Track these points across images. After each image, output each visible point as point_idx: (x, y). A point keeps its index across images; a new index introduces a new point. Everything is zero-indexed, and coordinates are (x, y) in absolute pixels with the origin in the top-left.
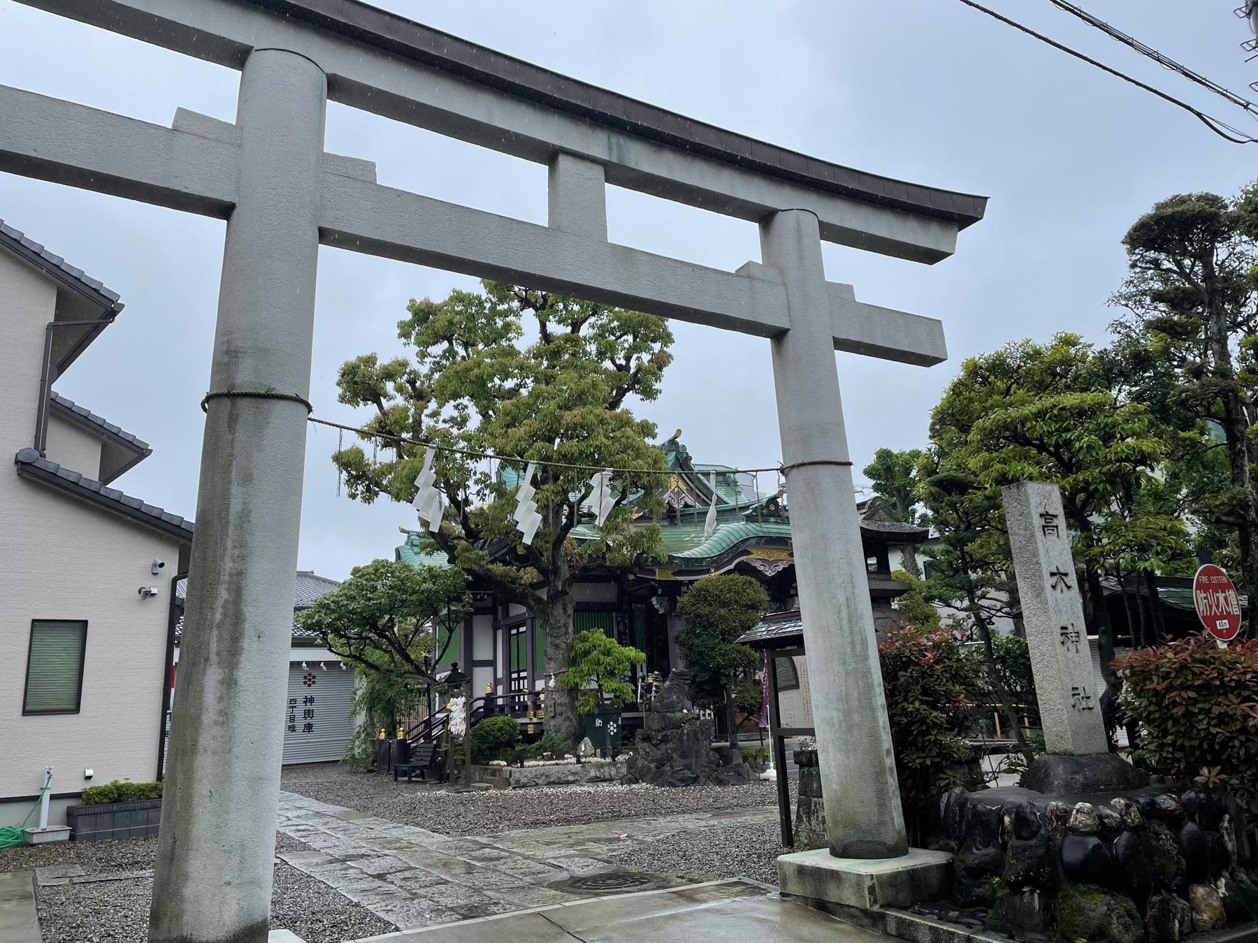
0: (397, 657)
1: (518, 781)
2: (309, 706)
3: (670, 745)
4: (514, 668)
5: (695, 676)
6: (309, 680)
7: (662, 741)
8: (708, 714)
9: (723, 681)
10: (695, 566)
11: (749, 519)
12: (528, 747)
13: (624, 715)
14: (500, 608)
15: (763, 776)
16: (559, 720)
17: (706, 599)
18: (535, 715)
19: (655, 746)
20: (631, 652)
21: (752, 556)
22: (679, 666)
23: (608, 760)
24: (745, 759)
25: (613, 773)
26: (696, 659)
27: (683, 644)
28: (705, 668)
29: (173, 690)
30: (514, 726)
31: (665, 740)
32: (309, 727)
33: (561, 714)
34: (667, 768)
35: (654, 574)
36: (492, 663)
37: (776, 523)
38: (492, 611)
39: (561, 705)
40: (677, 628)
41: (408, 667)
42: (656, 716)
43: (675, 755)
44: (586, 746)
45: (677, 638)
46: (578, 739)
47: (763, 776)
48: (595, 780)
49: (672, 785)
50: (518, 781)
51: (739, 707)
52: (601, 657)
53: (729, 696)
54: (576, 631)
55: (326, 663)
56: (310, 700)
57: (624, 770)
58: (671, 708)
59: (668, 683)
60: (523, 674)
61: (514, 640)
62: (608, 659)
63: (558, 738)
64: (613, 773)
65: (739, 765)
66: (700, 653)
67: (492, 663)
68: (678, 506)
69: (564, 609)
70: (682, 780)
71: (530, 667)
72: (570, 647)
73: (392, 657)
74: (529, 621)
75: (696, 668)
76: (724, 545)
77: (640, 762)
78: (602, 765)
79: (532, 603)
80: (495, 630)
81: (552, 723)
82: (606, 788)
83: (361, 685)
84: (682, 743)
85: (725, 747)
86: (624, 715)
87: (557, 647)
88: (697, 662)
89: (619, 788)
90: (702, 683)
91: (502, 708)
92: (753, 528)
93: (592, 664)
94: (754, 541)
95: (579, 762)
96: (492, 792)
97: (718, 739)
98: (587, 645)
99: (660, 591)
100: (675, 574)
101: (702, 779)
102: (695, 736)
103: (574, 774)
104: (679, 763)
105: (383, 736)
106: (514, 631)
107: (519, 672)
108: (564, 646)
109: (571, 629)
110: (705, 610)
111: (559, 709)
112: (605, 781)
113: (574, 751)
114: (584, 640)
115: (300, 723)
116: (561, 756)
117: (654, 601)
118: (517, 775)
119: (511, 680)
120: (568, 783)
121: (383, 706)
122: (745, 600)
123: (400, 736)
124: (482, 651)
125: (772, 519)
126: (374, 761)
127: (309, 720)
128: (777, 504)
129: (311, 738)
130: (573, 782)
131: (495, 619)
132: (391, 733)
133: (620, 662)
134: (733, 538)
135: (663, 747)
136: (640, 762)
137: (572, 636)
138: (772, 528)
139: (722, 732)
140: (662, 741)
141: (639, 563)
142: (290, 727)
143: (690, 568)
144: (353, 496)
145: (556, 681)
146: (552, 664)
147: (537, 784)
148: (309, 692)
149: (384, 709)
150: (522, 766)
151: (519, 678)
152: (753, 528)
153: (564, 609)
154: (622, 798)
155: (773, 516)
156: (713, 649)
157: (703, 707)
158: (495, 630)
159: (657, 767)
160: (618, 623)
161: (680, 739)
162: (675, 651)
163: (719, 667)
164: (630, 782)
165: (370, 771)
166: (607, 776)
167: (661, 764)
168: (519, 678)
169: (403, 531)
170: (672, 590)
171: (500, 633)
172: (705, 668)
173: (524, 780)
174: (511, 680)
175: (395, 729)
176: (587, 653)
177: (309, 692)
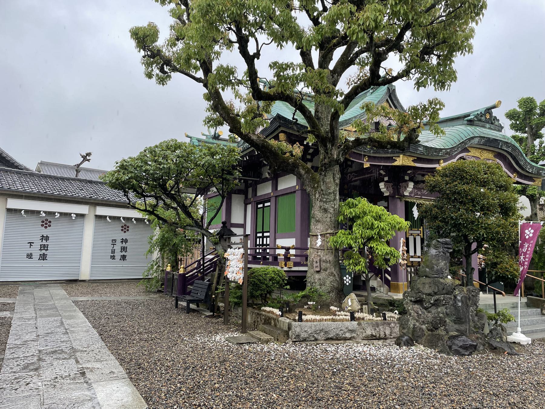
0: (183, 216)
1: (298, 336)
2: (124, 245)
4: (259, 229)
6: (125, 229)
7: (433, 305)
11: (471, 123)
14: (250, 190)
16: (323, 275)
18: (286, 265)
19: (426, 309)
21: (469, 154)
25: (388, 332)
29: (249, 242)
31: (436, 304)
32: (124, 258)
33: (325, 270)
36: (243, 226)
37: (490, 128)
38: (244, 192)
41: (188, 221)
44: (352, 301)
50: (298, 336)
55: (136, 219)
56: (125, 241)
60: (265, 234)
61: (260, 212)
63: (323, 290)
64: (388, 332)
71: (272, 230)
73: (178, 214)
74: (273, 200)
79: (303, 172)
80: (246, 205)
81: (317, 276)
83: (157, 233)
87: (326, 210)
95: (353, 318)
96: (274, 346)
99: (386, 179)
103: (352, 331)
104: (453, 329)
105: (169, 269)
106: (260, 206)
107: (263, 232)
108: (331, 210)
111: (324, 265)
112: (379, 339)
115: (118, 254)
118: (298, 330)
119: (257, 237)
120: (345, 339)
121: (171, 248)
123: (181, 271)
124: (237, 217)
125: (488, 125)
126: (162, 285)
127: (124, 253)
128: (491, 114)
129: (124, 264)
130: (350, 339)
131: (246, 197)
132: (175, 267)
134: (455, 140)
135: (433, 310)
140: (433, 305)
142: (111, 257)
144: (149, 76)
145: (323, 241)
146: (319, 226)
147: (316, 340)
148: (125, 236)
149: (170, 251)
151: (263, 237)
155: (488, 123)
158: (246, 205)
165: (159, 291)
166: (382, 335)
167: (434, 327)
168: (263, 237)
169: (187, 136)
171: (249, 207)
173: (304, 335)
174: (257, 237)
175: (177, 264)
177: (125, 236)
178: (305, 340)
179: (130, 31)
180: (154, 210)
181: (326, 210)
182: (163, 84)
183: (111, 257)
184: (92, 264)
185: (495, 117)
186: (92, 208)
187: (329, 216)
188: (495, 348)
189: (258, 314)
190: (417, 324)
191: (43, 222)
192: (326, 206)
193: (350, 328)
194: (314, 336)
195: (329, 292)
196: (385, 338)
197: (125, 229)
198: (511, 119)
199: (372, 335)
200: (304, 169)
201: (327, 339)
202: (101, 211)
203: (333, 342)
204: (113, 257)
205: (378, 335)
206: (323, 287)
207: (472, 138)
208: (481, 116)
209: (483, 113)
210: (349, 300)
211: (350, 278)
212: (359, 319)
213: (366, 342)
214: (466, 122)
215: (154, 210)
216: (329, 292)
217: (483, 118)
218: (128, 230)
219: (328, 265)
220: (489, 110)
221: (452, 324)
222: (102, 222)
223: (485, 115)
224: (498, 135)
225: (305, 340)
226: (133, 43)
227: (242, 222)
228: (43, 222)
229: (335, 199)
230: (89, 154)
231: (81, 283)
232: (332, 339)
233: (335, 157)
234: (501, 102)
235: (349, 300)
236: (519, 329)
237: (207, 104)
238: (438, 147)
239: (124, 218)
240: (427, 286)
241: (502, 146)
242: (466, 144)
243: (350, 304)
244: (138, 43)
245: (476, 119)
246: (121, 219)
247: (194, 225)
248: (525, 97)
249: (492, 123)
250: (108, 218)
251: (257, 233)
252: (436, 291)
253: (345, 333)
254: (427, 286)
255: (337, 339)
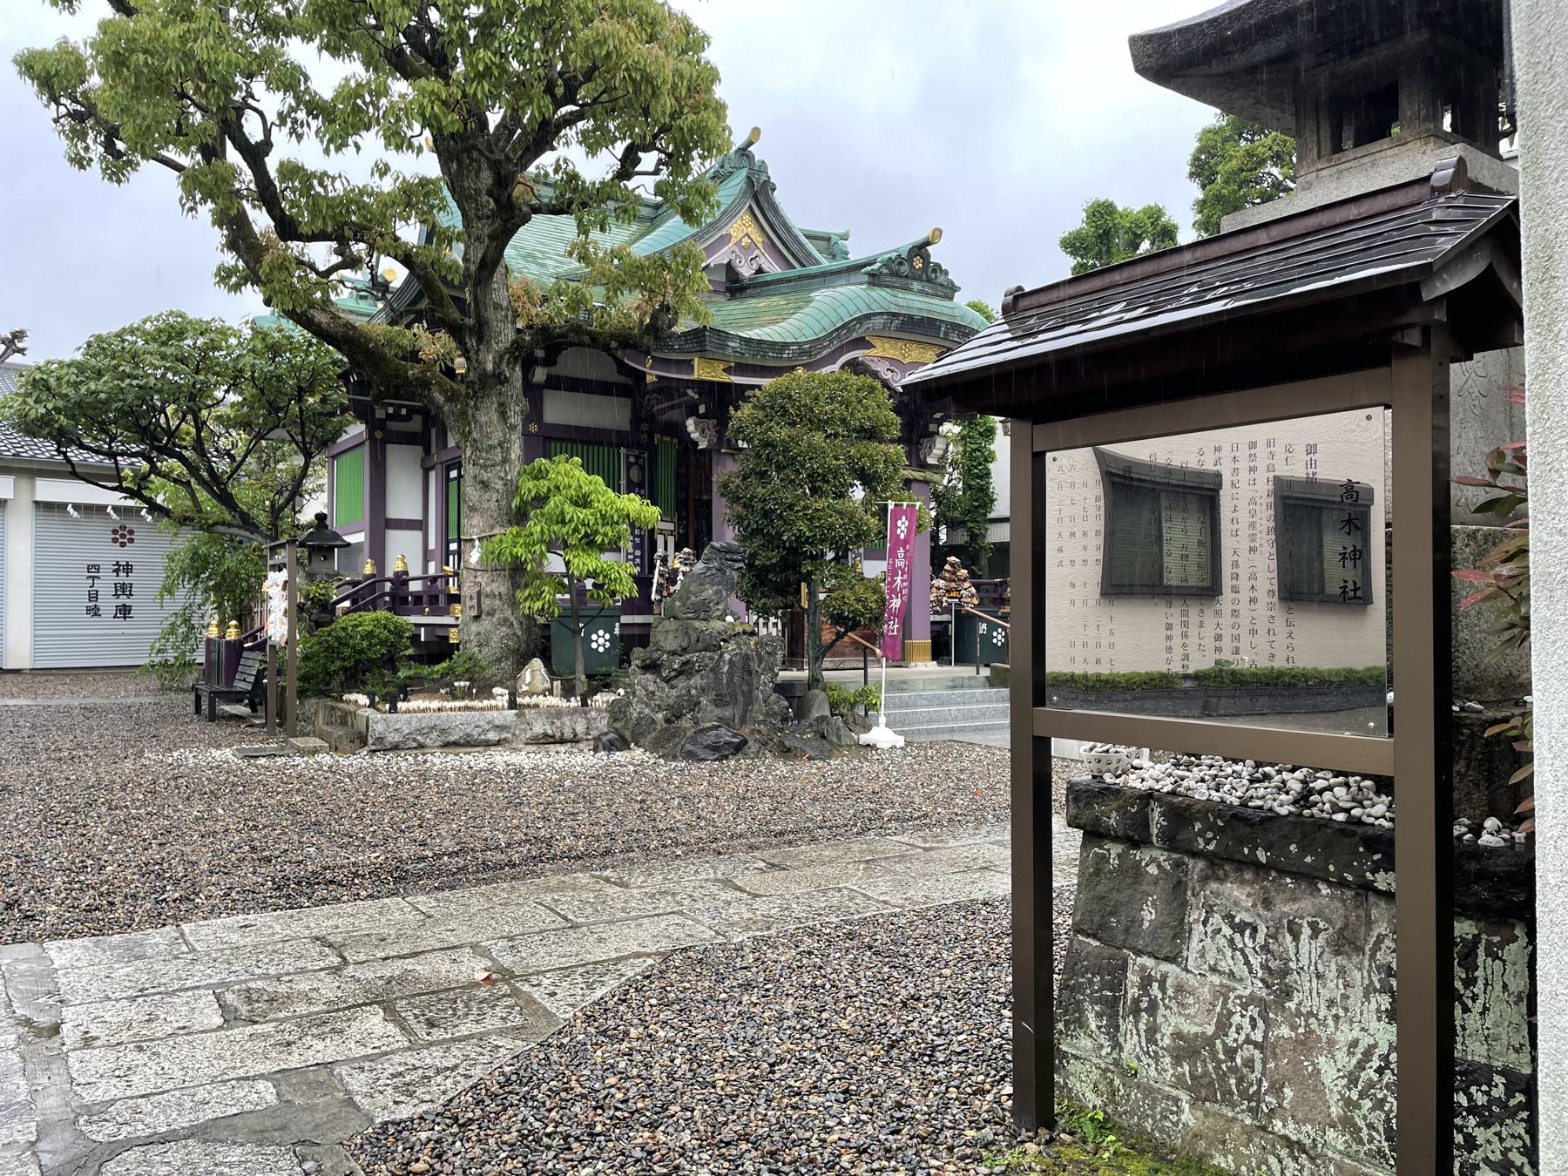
1: (380, 739)
3: (696, 680)
4: (453, 535)
5: (753, 556)
7: (680, 673)
8: (772, 628)
9: (807, 567)
10: (766, 358)
11: (875, 280)
12: (425, 670)
13: (625, 619)
15: (865, 738)
16: (486, 624)
17: (785, 412)
19: (667, 680)
20: (632, 503)
21: (872, 352)
22: (726, 535)
23: (575, 702)
24: (833, 706)
25: (580, 728)
26: (761, 524)
27: (735, 499)
28: (772, 541)
30: (398, 632)
31: (685, 671)
33: (491, 613)
34: (685, 723)
35: (688, 366)
39: (492, 596)
40: (725, 471)
42: (671, 625)
43: (704, 700)
45: (725, 486)
46: (522, 661)
47: (865, 738)
48: (546, 740)
49: (691, 756)
51: (832, 616)
52: (569, 510)
53: (812, 595)
54: (528, 458)
57: (603, 724)
58: (703, 611)
59: (700, 566)
61: (453, 485)
62: (583, 513)
64: (580, 728)
65: (823, 719)
66: (766, 514)
67: (420, 525)
68: (746, 271)
69: (503, 415)
70: (714, 748)
72: (512, 489)
75: (758, 541)
76: (817, 328)
77: (635, 711)
78: (558, 713)
80: (426, 472)
81: (474, 628)
82: (560, 757)
84: (717, 679)
85: (800, 681)
86: (625, 619)
87: (485, 485)
88: (758, 531)
89: (584, 760)
90: (766, 569)
91: (418, 598)
92: (883, 299)
93: (549, 521)
94: (879, 321)
95: (513, 704)
97: (789, 663)
98: (544, 485)
99: (702, 409)
100: (728, 370)
101: (753, 747)
102: (745, 665)
103: (501, 728)
104: (710, 713)
108: (499, 485)
109: (516, 451)
110: (780, 433)
112: (562, 741)
113: (511, 681)
114: (539, 475)
115: (108, 603)
116: (485, 691)
117: (690, 424)
120: (488, 744)
122: (859, 417)
125: (916, 285)
127: (123, 600)
128: (926, 258)
130: (498, 743)
131: (427, 452)
133: (605, 519)
134: (842, 311)
135: (681, 683)
136: (635, 711)
137: (516, 465)
138: (915, 302)
139: (794, 656)
140: (680, 673)
141: (657, 328)
142: (88, 609)
143: (758, 361)
144: (80, 162)
146: (476, 520)
147: (421, 746)
148: (123, 555)
150: (393, 709)
152: (883, 299)
153: (503, 415)
154: (583, 793)
155: (919, 279)
156: (791, 507)
157: (765, 612)
158: (426, 472)
159: (668, 721)
160: (629, 466)
161: (715, 670)
162: (721, 509)
163: (800, 540)
164: (611, 747)
166: (568, 734)
167: (675, 715)
170: (721, 399)
171: (432, 475)
172: (772, 541)
173: (393, 738)
174: (448, 553)
176: (541, 500)
177: (123, 555)
178: (395, 748)
179: (15, 61)
180: (140, 488)
181: (485, 485)
182: (119, 181)
183: (88, 609)
184: (36, 628)
185: (938, 265)
186: (24, 483)
187: (495, 496)
188: (789, 750)
189: (333, 708)
190: (647, 711)
191: (115, 532)
192: (485, 476)
193: (497, 722)
194: (415, 740)
195: (499, 660)
196: (575, 740)
197: (123, 536)
198: (1074, 253)
199: (546, 735)
200: (444, 392)
201: (447, 745)
202: (48, 490)
203: (459, 750)
204: (94, 611)
205: (558, 735)
206: (485, 650)
207: (868, 317)
208: (901, 264)
209: (904, 255)
210: (528, 673)
211: (607, 636)
212: (523, 706)
213: (534, 748)
214: (866, 278)
215: (140, 488)
216: (499, 660)
217: (905, 269)
218: (131, 541)
219: (497, 602)
220: (920, 249)
221: (711, 707)
222: (54, 519)
223: (910, 259)
224: (945, 311)
225: (395, 748)
226: (29, 88)
227: (418, 516)
228: (115, 532)
229: (505, 461)
230: (18, 335)
231: (9, 677)
232: (456, 744)
233: (490, 367)
234: (941, 231)
235: (528, 673)
236: (882, 720)
237: (219, 235)
238: (778, 339)
239: (76, 507)
240: (671, 636)
241: (946, 333)
242: (850, 331)
243: (528, 680)
244: (41, 85)
245: (885, 271)
246: (109, 510)
247: (238, 521)
248: (1102, 199)
249: (928, 281)
250: (70, 508)
251: (448, 543)
252: (685, 644)
253: (485, 732)
254: (671, 636)
255: (468, 744)
